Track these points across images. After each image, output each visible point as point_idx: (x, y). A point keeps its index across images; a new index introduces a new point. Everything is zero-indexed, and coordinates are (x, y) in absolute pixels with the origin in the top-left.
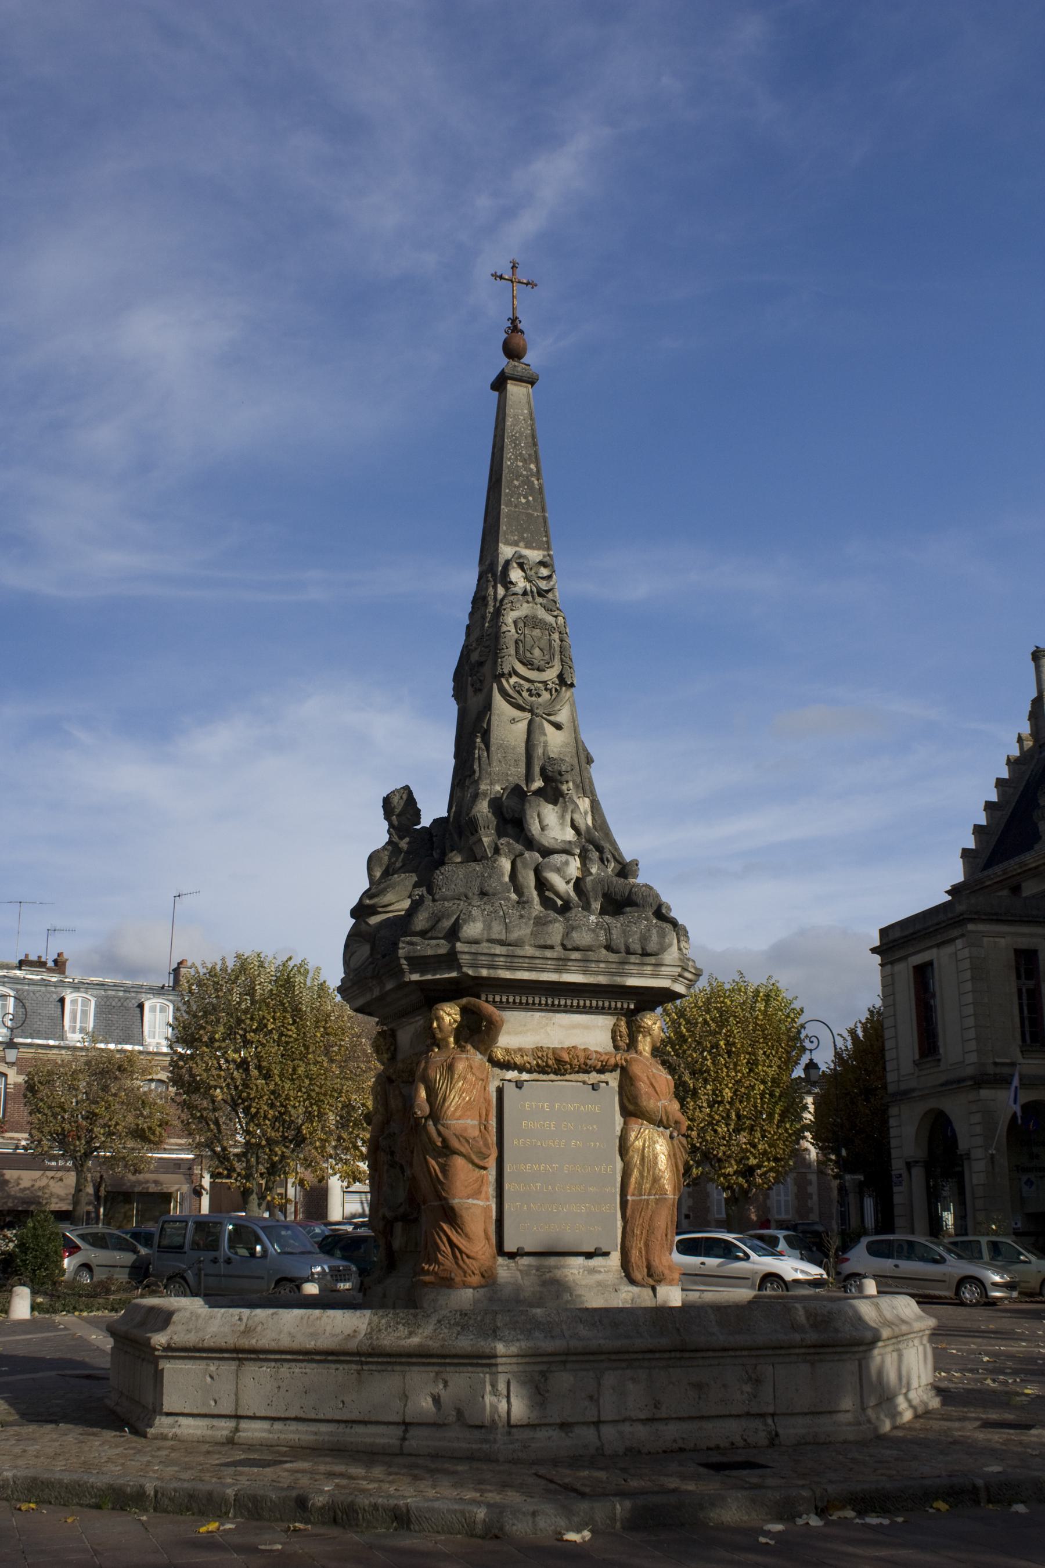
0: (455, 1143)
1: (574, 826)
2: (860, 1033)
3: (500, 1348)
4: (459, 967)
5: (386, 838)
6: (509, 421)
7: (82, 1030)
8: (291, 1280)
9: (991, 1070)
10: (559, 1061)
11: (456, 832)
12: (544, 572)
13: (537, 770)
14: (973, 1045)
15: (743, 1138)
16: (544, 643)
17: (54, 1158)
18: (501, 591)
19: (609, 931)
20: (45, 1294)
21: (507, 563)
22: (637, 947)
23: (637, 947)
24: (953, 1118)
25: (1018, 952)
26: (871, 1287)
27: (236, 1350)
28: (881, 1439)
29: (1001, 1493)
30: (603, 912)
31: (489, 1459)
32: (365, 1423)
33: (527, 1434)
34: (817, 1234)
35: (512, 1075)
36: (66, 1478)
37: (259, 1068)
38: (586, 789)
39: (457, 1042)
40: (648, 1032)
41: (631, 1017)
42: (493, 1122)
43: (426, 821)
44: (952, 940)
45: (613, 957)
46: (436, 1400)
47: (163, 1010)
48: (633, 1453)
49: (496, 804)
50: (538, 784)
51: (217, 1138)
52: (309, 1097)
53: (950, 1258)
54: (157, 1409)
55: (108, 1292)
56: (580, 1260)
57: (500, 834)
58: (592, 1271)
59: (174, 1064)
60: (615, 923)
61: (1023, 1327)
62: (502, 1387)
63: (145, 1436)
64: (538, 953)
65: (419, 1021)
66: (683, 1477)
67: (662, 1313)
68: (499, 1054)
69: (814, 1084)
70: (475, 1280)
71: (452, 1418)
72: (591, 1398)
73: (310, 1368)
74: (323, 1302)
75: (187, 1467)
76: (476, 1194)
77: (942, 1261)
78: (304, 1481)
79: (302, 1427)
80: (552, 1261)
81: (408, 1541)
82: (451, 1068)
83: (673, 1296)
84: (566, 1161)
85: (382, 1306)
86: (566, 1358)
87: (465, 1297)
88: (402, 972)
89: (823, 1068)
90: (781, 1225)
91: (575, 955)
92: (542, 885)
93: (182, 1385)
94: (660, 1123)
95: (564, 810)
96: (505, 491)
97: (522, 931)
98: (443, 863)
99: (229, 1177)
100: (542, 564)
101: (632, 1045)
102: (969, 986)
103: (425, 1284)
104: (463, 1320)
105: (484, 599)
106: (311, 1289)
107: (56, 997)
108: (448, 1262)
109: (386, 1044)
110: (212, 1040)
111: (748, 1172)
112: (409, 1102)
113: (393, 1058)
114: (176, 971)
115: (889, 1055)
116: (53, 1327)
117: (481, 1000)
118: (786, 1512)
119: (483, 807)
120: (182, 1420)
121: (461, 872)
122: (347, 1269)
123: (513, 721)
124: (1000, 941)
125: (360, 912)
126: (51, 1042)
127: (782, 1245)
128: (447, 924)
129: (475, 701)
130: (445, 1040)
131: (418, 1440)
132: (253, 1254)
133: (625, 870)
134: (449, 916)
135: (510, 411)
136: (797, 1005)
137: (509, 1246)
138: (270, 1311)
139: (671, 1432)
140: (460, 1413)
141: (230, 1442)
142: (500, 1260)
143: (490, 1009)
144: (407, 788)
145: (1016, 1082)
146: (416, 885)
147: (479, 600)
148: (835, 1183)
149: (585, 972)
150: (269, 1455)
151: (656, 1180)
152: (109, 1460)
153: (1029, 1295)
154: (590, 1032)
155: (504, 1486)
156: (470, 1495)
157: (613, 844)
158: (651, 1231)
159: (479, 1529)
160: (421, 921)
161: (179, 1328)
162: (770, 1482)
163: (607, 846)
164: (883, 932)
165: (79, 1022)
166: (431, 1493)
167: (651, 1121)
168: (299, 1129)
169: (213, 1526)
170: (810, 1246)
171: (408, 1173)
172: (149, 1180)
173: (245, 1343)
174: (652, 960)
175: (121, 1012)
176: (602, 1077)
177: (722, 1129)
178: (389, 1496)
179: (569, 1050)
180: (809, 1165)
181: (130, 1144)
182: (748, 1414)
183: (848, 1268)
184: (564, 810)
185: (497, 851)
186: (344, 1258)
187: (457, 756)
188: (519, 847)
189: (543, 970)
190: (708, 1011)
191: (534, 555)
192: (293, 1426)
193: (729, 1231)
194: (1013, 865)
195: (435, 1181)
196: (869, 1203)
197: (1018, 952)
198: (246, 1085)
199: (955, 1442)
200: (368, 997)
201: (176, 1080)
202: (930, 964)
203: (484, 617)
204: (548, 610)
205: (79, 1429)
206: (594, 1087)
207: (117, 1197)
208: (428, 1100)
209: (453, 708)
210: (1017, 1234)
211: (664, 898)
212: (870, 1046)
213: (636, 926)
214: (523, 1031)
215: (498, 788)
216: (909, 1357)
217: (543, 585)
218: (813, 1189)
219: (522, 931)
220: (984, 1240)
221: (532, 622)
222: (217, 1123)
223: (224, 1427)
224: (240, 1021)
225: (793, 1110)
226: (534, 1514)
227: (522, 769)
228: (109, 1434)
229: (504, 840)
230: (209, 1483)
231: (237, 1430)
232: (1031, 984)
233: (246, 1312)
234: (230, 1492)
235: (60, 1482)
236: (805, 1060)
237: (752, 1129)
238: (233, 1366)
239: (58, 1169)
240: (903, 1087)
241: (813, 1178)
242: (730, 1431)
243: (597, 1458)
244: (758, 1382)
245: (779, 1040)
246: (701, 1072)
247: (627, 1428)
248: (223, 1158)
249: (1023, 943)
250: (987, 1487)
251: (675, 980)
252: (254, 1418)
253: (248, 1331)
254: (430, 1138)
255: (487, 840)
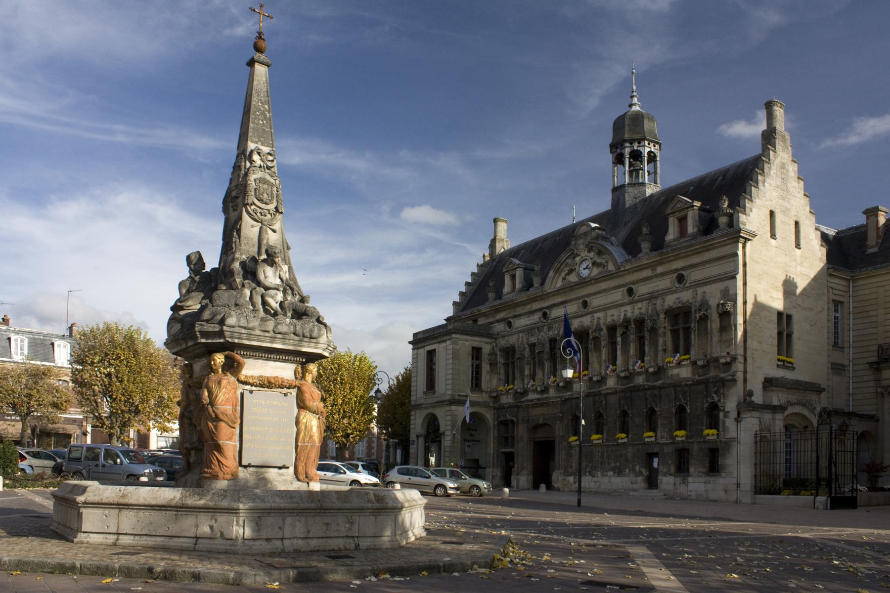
0: (221, 416)
1: (280, 278)
2: (400, 378)
3: (241, 506)
4: (225, 338)
5: (188, 275)
6: (255, 83)
7: (22, 354)
8: (134, 475)
9: (457, 398)
10: (269, 382)
11: (223, 275)
12: (270, 158)
13: (263, 250)
14: (450, 387)
15: (346, 421)
16: (269, 191)
17: (10, 415)
18: (248, 164)
19: (295, 326)
20: (10, 479)
21: (252, 151)
22: (308, 334)
23: (308, 334)
24: (439, 417)
25: (473, 348)
26: (398, 486)
27: (118, 504)
28: (401, 547)
29: (449, 568)
30: (292, 318)
31: (234, 553)
32: (178, 537)
33: (252, 543)
34: (375, 464)
35: (248, 387)
36: (36, 560)
37: (117, 377)
38: (286, 261)
39: (223, 371)
40: (311, 372)
41: (303, 364)
42: (239, 408)
43: (208, 269)
44: (445, 341)
45: (296, 338)
46: (211, 528)
47: (65, 347)
48: (298, 552)
49: (243, 264)
50: (264, 256)
51: (96, 408)
52: (142, 392)
53: (433, 477)
54: (79, 530)
55: (43, 479)
56: (276, 470)
57: (245, 278)
58: (281, 475)
59: (73, 373)
60: (298, 324)
61: (461, 505)
62: (241, 522)
63: (72, 542)
64: (262, 334)
65: (204, 361)
66: (319, 561)
67: (311, 493)
68: (242, 378)
69: (378, 399)
70: (229, 476)
71: (218, 535)
72: (280, 528)
73: (153, 513)
74: (152, 483)
75: (95, 555)
76: (230, 439)
77: (429, 477)
78: (151, 561)
79: (149, 538)
80: (264, 470)
81: (199, 586)
82: (220, 383)
83: (316, 486)
84: (271, 428)
85: (184, 486)
86: (270, 511)
87: (222, 484)
88: (197, 338)
89: (383, 392)
90: (359, 460)
91: (279, 336)
92: (264, 303)
93: (91, 519)
94: (314, 412)
95: (276, 270)
96: (252, 116)
97: (255, 323)
98: (217, 289)
99: (102, 427)
100: (269, 154)
101: (303, 377)
102: (451, 361)
103: (206, 478)
104: (224, 493)
105: (240, 166)
106: (144, 479)
107: (6, 337)
108: (217, 469)
109: (188, 370)
110: (93, 363)
111: (347, 436)
112: (199, 398)
113: (191, 377)
114: (71, 328)
115: (413, 389)
116: (16, 494)
117: (234, 353)
118: (361, 575)
119: (236, 265)
120: (91, 535)
121: (226, 294)
122: (161, 471)
123: (252, 226)
124: (466, 343)
125: (175, 308)
126: (5, 359)
127: (360, 468)
128: (219, 317)
129: (233, 215)
130: (217, 370)
131: (203, 544)
132: (116, 463)
133: (303, 300)
134: (220, 314)
135: (256, 78)
136: (374, 365)
137: (244, 463)
138: (135, 487)
139: (314, 543)
140: (222, 534)
141: (115, 544)
142: (240, 468)
143: (238, 357)
144: (198, 252)
145: (468, 404)
146: (203, 298)
147: (237, 167)
148: (384, 443)
149: (283, 344)
150: (133, 551)
151: (311, 437)
152: (57, 552)
153: (464, 493)
154: (285, 371)
155: (241, 564)
156: (226, 568)
157: (298, 287)
158: (308, 458)
159: (231, 581)
160: (206, 315)
161: (90, 494)
162: (356, 563)
163: (295, 288)
164: (415, 335)
165: (19, 352)
166: (209, 566)
167: (310, 411)
168: (137, 407)
169: (109, 580)
170: (372, 468)
171: (198, 428)
172: (60, 427)
173: (122, 501)
174: (314, 340)
175: (42, 347)
176: (289, 391)
177: (336, 417)
178: (190, 568)
179: (274, 378)
180: (374, 434)
181: (51, 410)
182: (347, 537)
183: (389, 479)
184: (276, 270)
185: (243, 286)
186: (159, 466)
187: (224, 239)
188: (254, 285)
189: (264, 342)
190: (333, 364)
191: (266, 149)
192: (145, 538)
193: (337, 461)
194: (475, 310)
195: (211, 432)
196: (399, 452)
197: (473, 348)
198: (110, 385)
199: (432, 549)
200: (179, 348)
201: (75, 381)
202: (435, 350)
203: (239, 176)
204: (272, 176)
205: (39, 539)
206: (285, 395)
207: (44, 435)
208: (209, 396)
209: (222, 218)
210: (461, 467)
211: (321, 314)
212: (404, 384)
213: (308, 325)
214: (253, 368)
215: (244, 257)
216: (415, 514)
217: (270, 164)
218: (375, 445)
219: (255, 323)
220: (448, 469)
221: (262, 181)
222: (96, 402)
223: (111, 539)
224: (107, 355)
225: (368, 410)
226: (255, 575)
227: (256, 249)
228: (55, 541)
229: (247, 281)
230: (107, 562)
231: (118, 539)
232: (478, 362)
233: (123, 488)
234: (117, 566)
235: (33, 562)
236: (375, 388)
237: (350, 417)
238: (117, 511)
239: (12, 420)
240: (418, 402)
241: (375, 440)
242: (339, 543)
243: (282, 553)
244: (352, 523)
245: (364, 379)
246: (328, 391)
247: (295, 541)
248: (99, 418)
249: (476, 344)
250: (444, 566)
251: (324, 350)
252: (126, 534)
253: (123, 496)
254: (209, 413)
255: (238, 280)
